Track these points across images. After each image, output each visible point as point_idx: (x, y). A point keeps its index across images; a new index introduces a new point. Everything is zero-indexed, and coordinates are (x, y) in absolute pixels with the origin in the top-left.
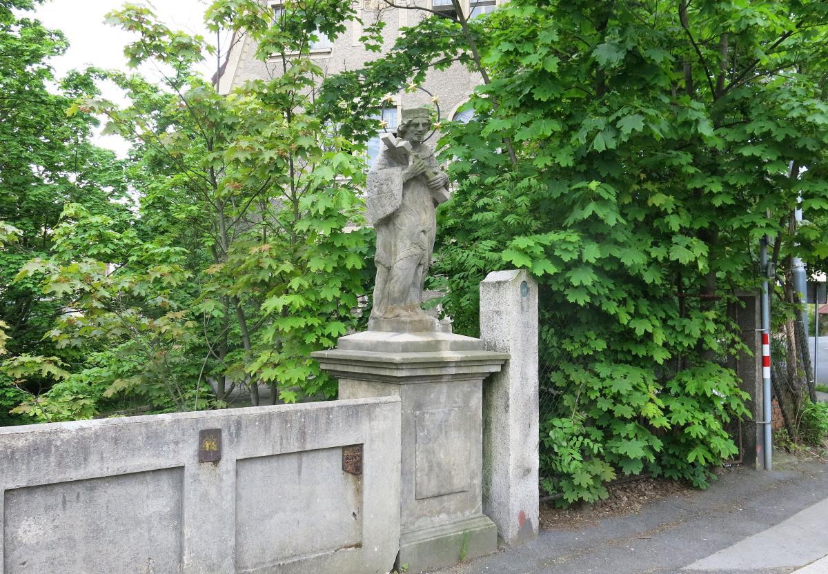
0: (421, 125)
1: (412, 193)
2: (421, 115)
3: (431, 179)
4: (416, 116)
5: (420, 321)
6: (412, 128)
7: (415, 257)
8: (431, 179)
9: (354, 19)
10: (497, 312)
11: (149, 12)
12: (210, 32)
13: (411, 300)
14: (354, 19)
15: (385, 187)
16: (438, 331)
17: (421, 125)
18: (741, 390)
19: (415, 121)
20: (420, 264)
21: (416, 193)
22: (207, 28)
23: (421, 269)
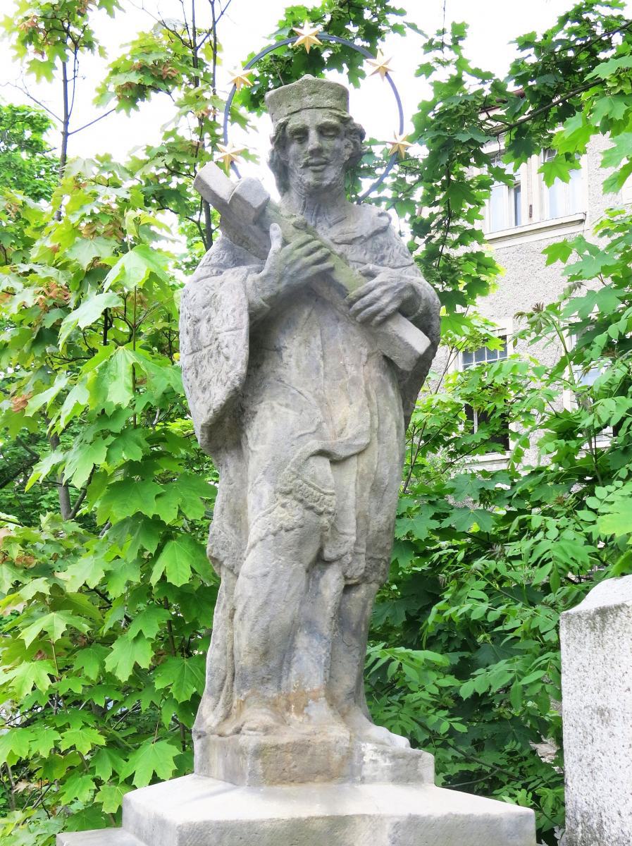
0: (313, 134)
1: (307, 342)
2: (309, 100)
3: (353, 294)
4: (295, 105)
5: (300, 748)
6: (294, 148)
7: (289, 537)
8: (353, 294)
9: (408, 30)
10: (601, 712)
11: (537, 339)
12: (38, 80)
13: (300, 677)
14: (408, 30)
15: (203, 326)
16: (374, 780)
17: (313, 134)
18: (468, 772)
19: (295, 123)
20: (321, 561)
21: (317, 341)
22: (30, 71)
23: (332, 581)
